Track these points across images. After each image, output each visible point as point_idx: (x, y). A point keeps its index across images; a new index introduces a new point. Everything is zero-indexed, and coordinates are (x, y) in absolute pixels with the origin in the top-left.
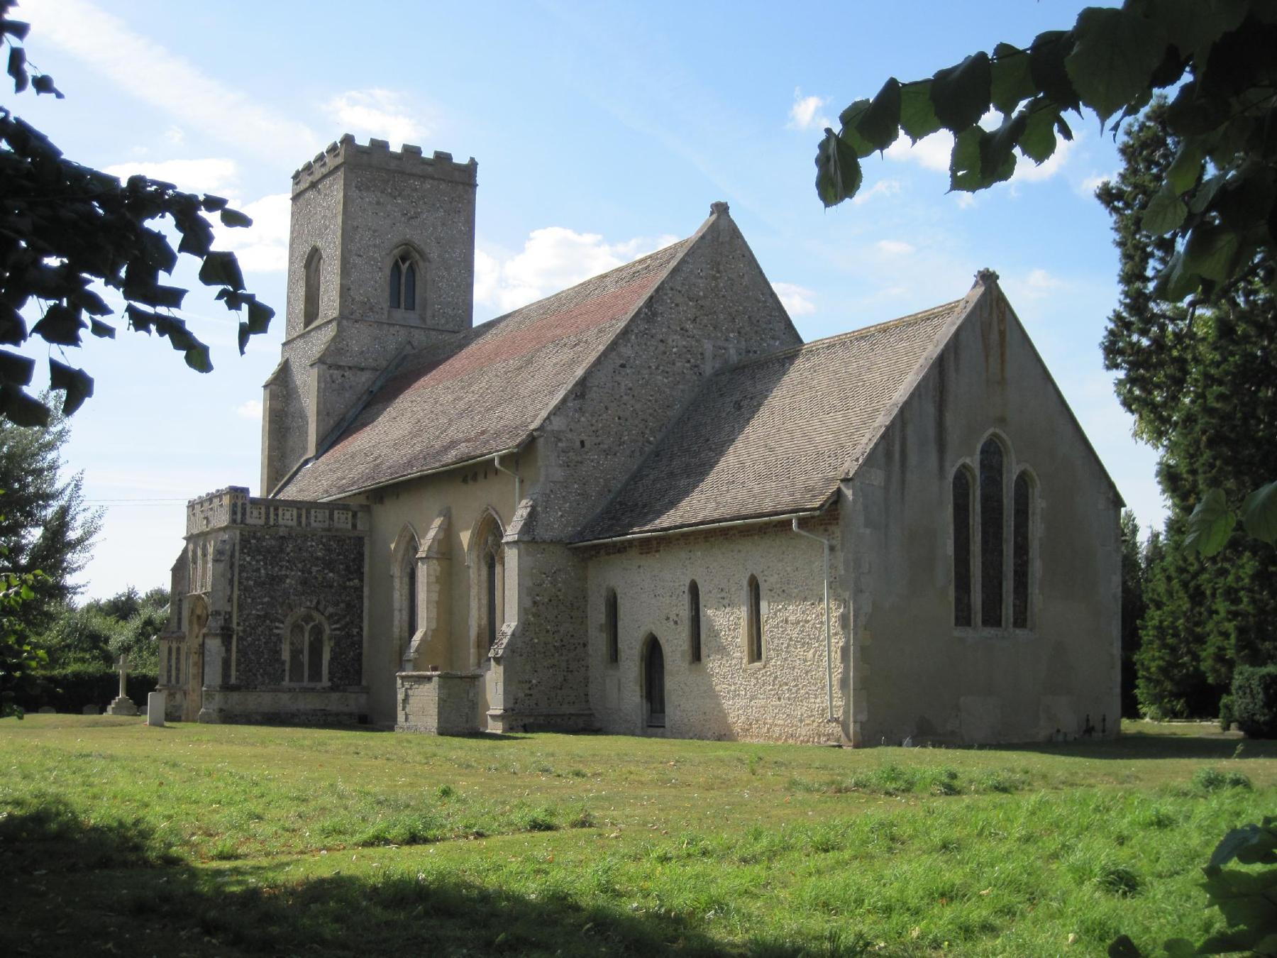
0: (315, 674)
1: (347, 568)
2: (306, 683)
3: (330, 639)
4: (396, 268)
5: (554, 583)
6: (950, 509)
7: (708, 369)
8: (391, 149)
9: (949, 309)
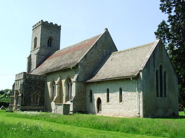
1: (42, 86)
3: (39, 97)
4: (49, 41)
5: (81, 88)
6: (156, 76)
7: (104, 54)
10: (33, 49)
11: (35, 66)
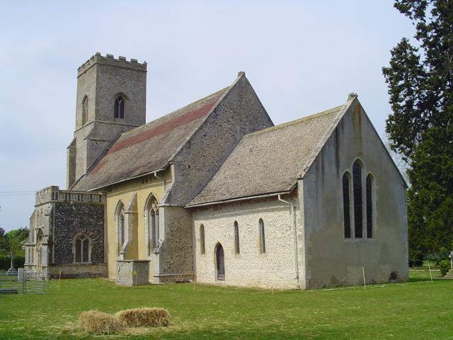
0: (86, 259)
2: (82, 262)
4: (117, 103)
5: (179, 222)
8: (115, 58)
9: (338, 110)
10: (81, 127)
11: (85, 168)
